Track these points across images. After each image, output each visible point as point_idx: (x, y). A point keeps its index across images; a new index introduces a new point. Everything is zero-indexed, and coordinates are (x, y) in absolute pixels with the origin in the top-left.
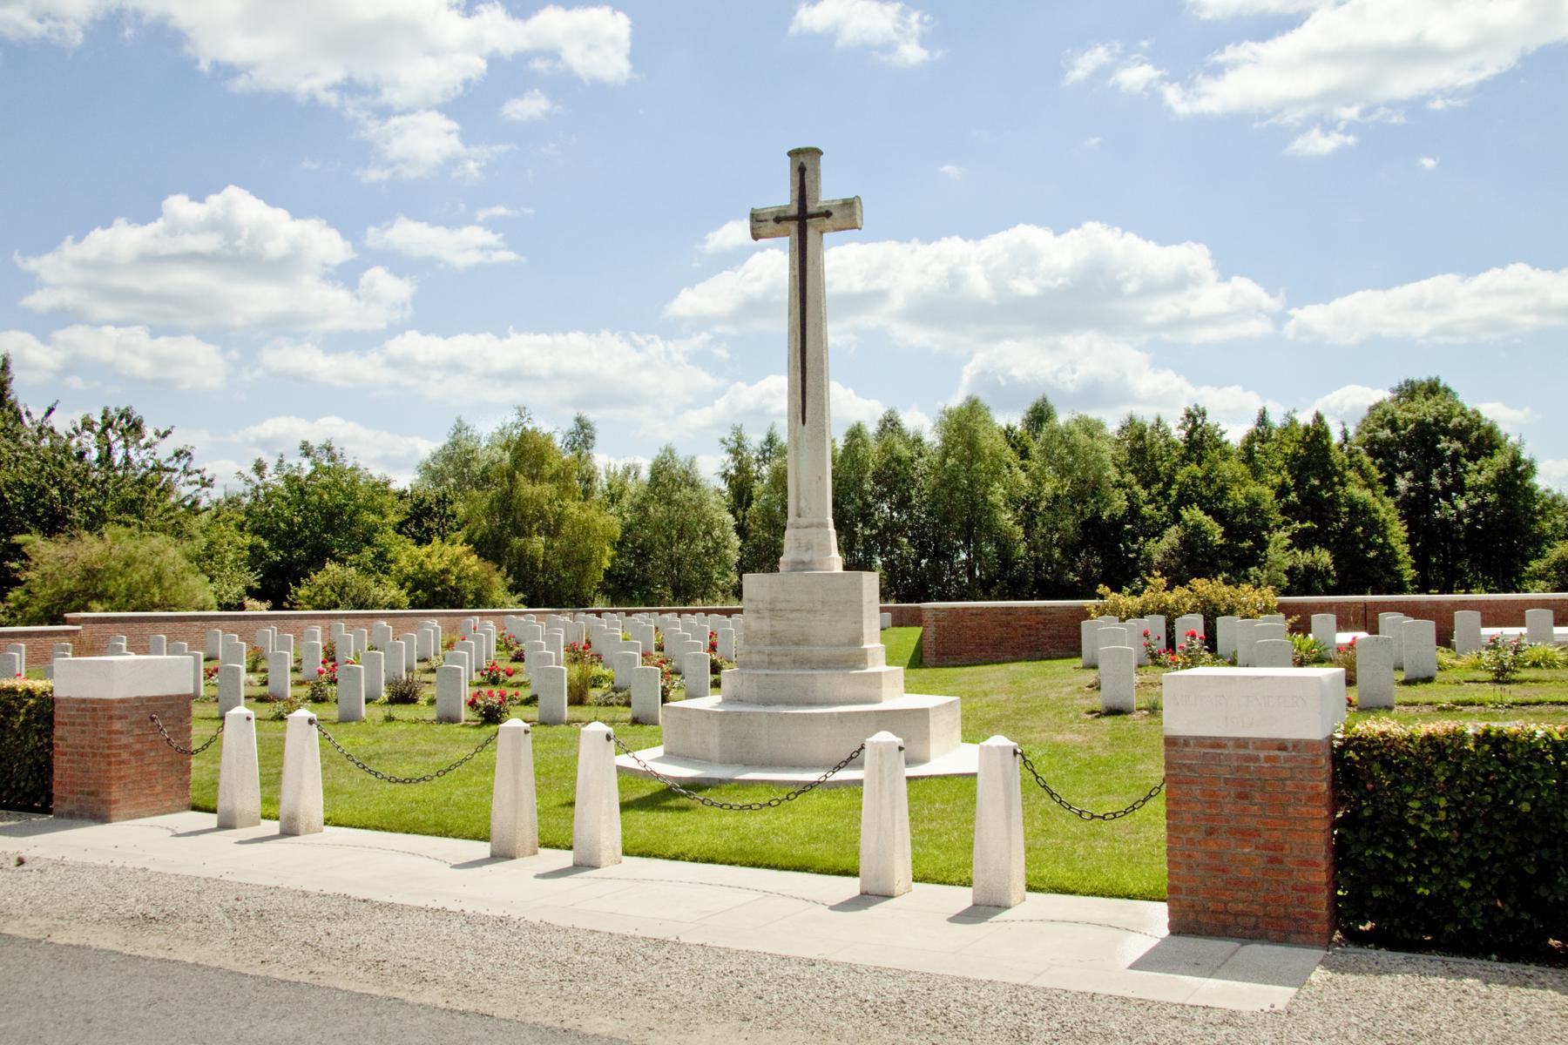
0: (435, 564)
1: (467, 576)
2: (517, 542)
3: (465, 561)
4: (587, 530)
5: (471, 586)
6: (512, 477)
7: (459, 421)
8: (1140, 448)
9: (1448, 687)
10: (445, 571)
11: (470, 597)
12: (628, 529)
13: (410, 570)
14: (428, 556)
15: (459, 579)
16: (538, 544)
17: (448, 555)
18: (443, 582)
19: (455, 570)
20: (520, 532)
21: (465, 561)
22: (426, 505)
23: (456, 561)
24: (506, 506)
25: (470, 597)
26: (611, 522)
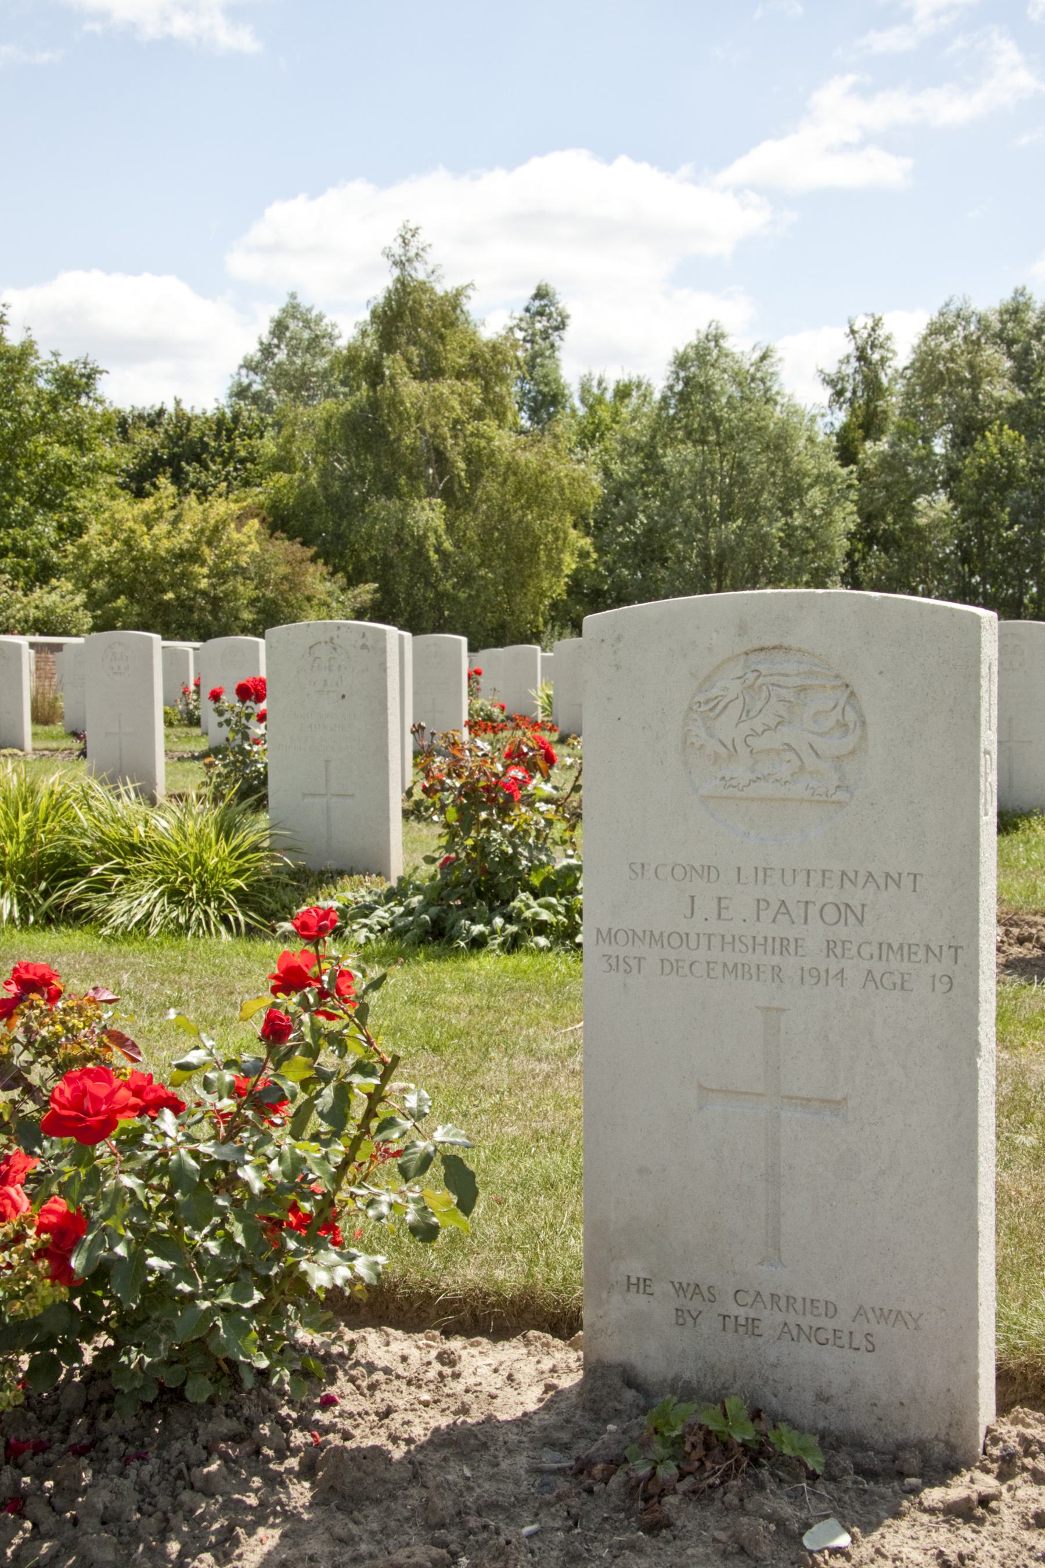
0: (160, 540)
1: (239, 571)
2: (382, 506)
3: (233, 534)
4: (532, 490)
5: (246, 590)
6: (374, 373)
7: (293, 296)
8: (446, 960)
9: (187, 765)
10: (191, 556)
11: (247, 615)
12: (618, 491)
13: (105, 553)
14: (149, 521)
15: (220, 575)
16: (428, 514)
17: (226, 525)
18: (186, 577)
19: (209, 555)
20: (389, 489)
21: (233, 534)
22: (194, 434)
23: (213, 535)
24: (368, 432)
25: (247, 615)
26: (585, 475)
